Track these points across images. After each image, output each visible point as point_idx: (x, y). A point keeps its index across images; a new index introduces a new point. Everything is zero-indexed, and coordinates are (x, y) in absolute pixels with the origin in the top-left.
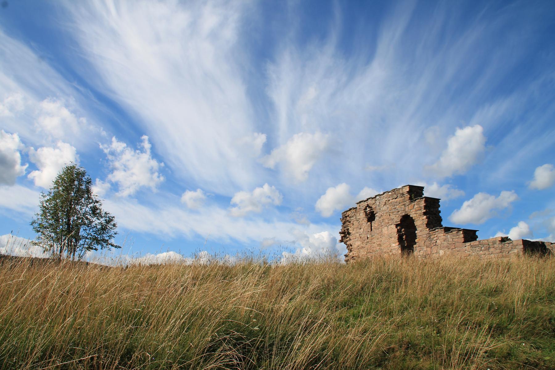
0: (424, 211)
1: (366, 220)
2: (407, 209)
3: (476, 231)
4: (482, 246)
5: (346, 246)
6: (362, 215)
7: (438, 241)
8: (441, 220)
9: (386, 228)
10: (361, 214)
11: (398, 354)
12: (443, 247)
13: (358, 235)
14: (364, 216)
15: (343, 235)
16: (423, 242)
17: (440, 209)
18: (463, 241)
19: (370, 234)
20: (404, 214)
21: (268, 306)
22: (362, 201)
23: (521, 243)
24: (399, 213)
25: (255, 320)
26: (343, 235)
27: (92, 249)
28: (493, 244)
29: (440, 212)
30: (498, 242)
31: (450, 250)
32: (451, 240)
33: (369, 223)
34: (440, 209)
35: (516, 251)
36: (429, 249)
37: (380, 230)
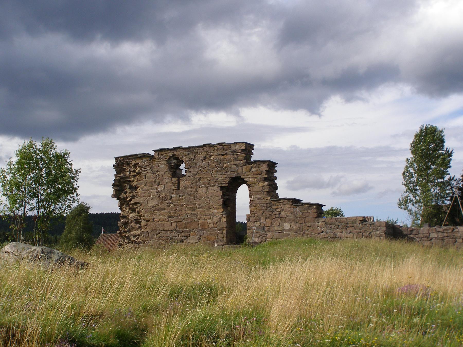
1: (169, 174)
2: (240, 171)
4: (339, 224)
7: (282, 213)
8: (277, 188)
9: (204, 189)
10: (162, 166)
12: (290, 220)
13: (154, 192)
14: (167, 169)
15: (117, 188)
16: (261, 212)
18: (316, 216)
19: (177, 194)
20: (234, 175)
21: (384, 235)
22: (179, 148)
23: (385, 225)
24: (229, 173)
26: (117, 188)
27: (406, 208)
29: (276, 178)
30: (358, 222)
31: (298, 224)
32: (301, 213)
33: (174, 179)
34: (276, 175)
36: (268, 220)
37: (194, 190)
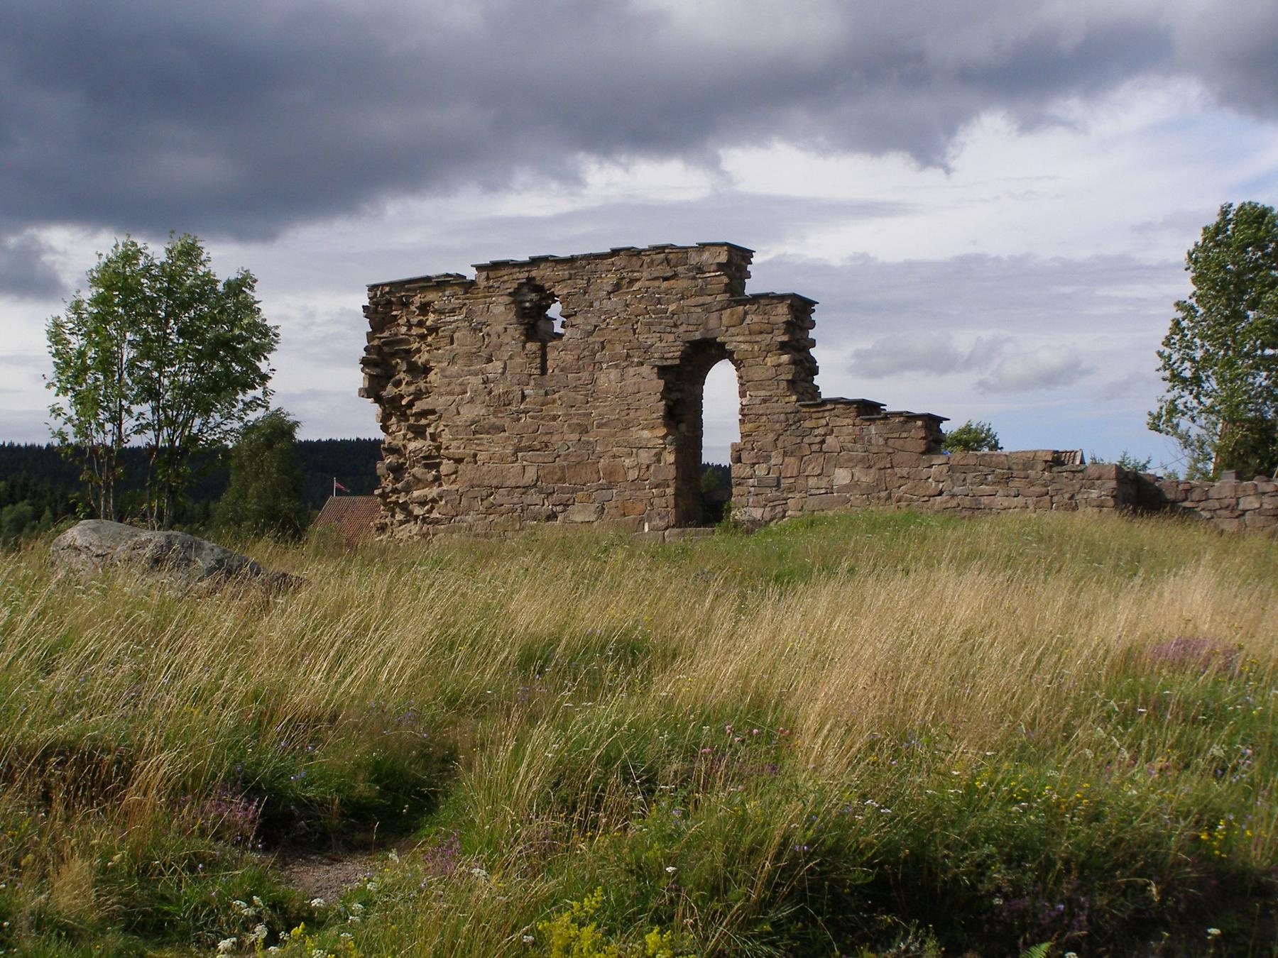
0: (785, 338)
1: (516, 332)
3: (941, 420)
4: (987, 470)
5: (376, 409)
6: (500, 312)
7: (829, 439)
8: (815, 371)
9: (614, 375)
10: (499, 309)
11: (1232, 817)
13: (475, 381)
14: (511, 316)
16: (771, 436)
17: (812, 334)
20: (697, 336)
22: (545, 259)
24: (682, 329)
25: (1062, 907)
28: (1025, 469)
30: (1040, 467)
31: (872, 471)
32: (881, 441)
33: (532, 346)
34: (812, 334)
35: (1094, 494)
37: (585, 375)
